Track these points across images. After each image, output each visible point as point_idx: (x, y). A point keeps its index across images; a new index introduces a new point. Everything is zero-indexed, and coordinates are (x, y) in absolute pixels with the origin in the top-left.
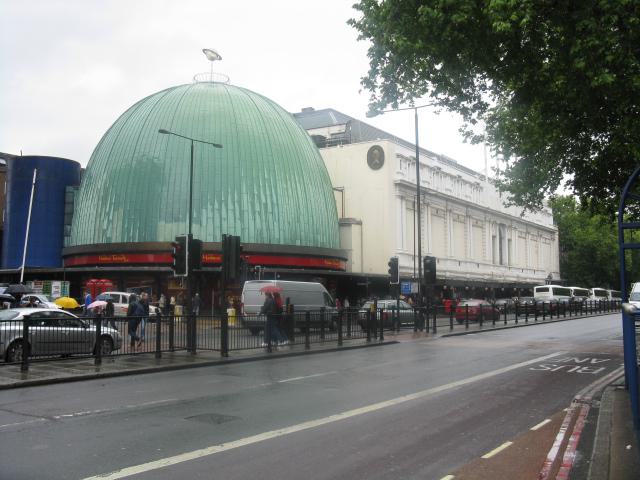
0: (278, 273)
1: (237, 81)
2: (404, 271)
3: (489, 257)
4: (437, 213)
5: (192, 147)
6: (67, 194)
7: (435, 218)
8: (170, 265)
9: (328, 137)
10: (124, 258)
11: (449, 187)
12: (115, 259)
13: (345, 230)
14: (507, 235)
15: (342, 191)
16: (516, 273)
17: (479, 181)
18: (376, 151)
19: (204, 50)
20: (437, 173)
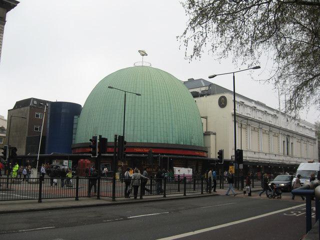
3: (281, 151)
9: (200, 92)
13: (208, 137)
14: (291, 141)
17: (276, 114)
19: (139, 51)
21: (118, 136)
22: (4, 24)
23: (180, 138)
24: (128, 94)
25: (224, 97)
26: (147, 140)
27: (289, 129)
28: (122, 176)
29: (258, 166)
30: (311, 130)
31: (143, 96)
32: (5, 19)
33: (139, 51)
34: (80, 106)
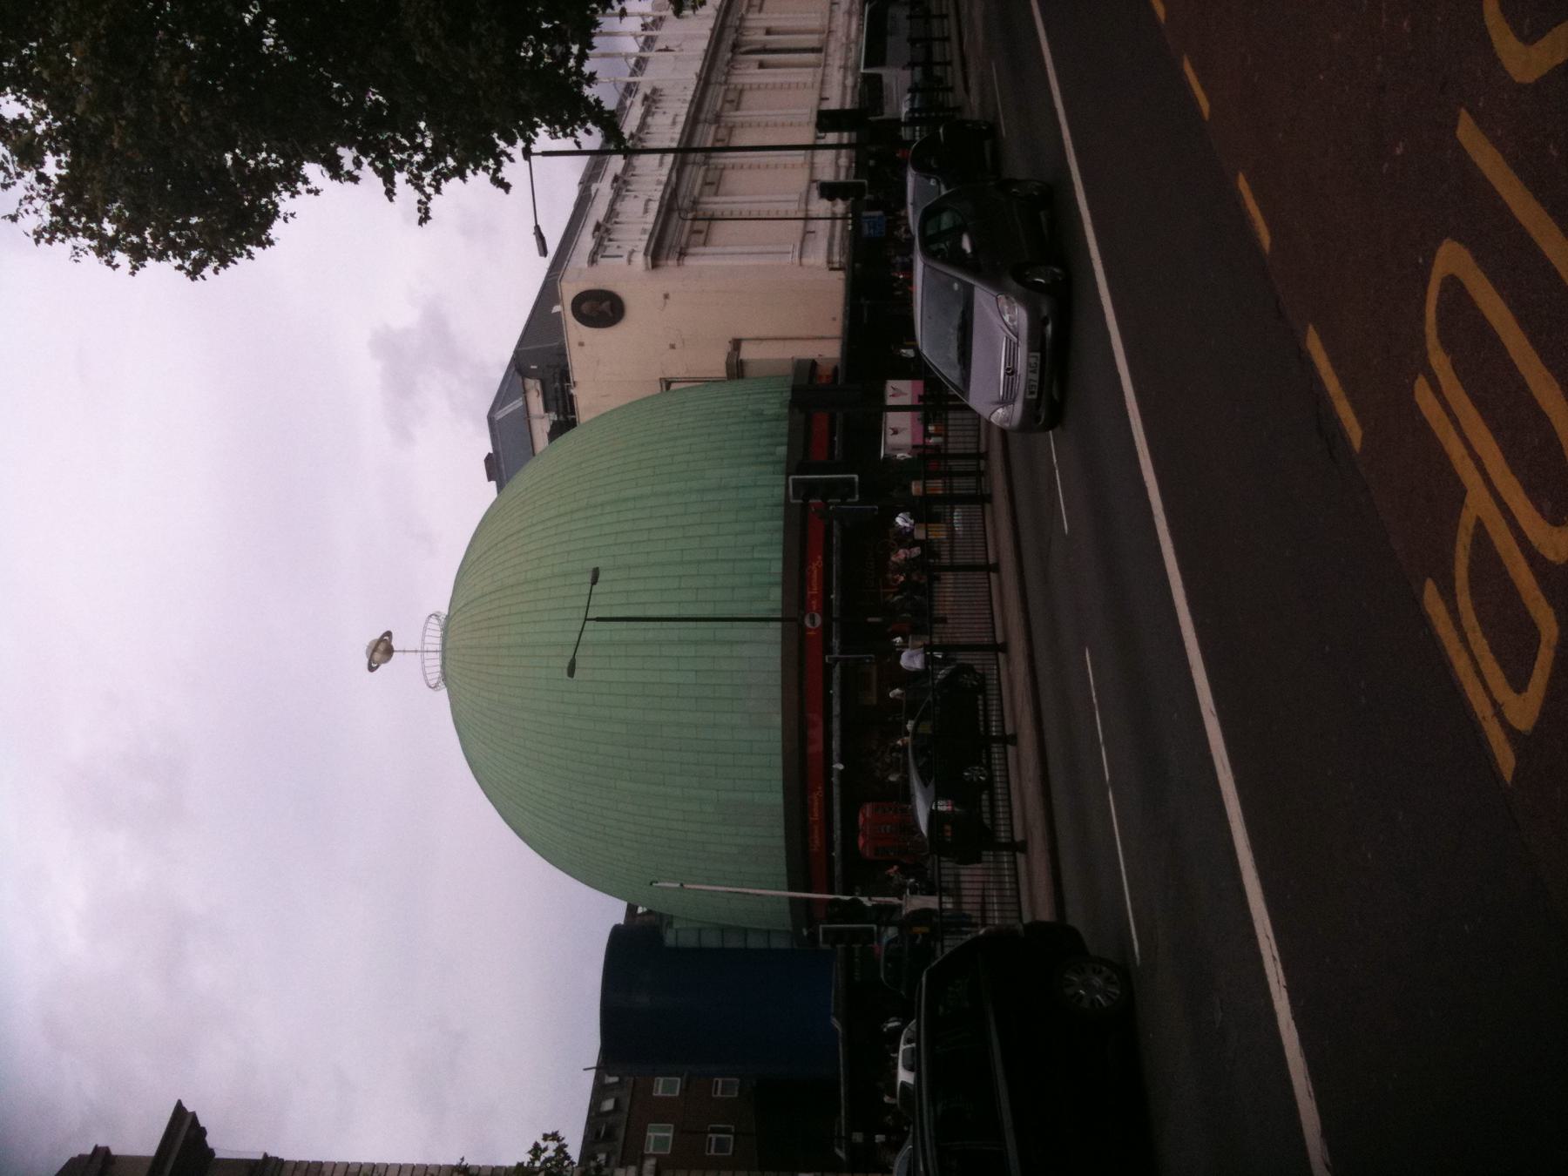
1: (440, 599)
2: (848, 98)
3: (806, 76)
4: (714, 184)
5: (598, 619)
7: (722, 189)
9: (553, 416)
10: (833, 596)
11: (640, 204)
12: (816, 814)
13: (748, 371)
14: (759, 37)
16: (840, 19)
17: (639, 98)
18: (585, 307)
19: (371, 669)
20: (626, 183)
22: (280, 1163)
25: (579, 301)
26: (771, 584)
27: (704, 44)
29: (872, 163)
30: (621, 184)
31: (600, 563)
32: (256, 1162)
33: (371, 669)
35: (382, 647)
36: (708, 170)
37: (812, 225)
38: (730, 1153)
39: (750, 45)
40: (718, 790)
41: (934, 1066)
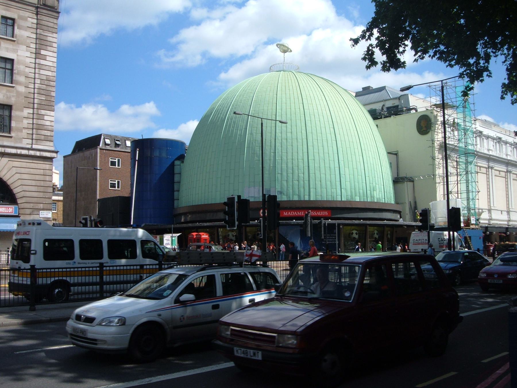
0: (70, 256)
5: (262, 124)
6: (175, 167)
8: (224, 220)
15: (396, 154)
21: (267, 196)
23: (353, 191)
24: (264, 121)
28: (299, 260)
31: (288, 125)
33: (291, 51)
34: (183, 144)
35: (286, 49)
36: (486, 168)
37: (505, 213)
38: (110, 188)
39: (218, 103)
40: (221, 177)
41: (405, 248)
